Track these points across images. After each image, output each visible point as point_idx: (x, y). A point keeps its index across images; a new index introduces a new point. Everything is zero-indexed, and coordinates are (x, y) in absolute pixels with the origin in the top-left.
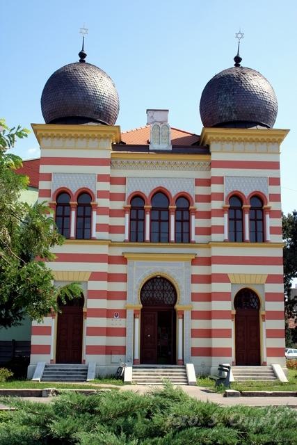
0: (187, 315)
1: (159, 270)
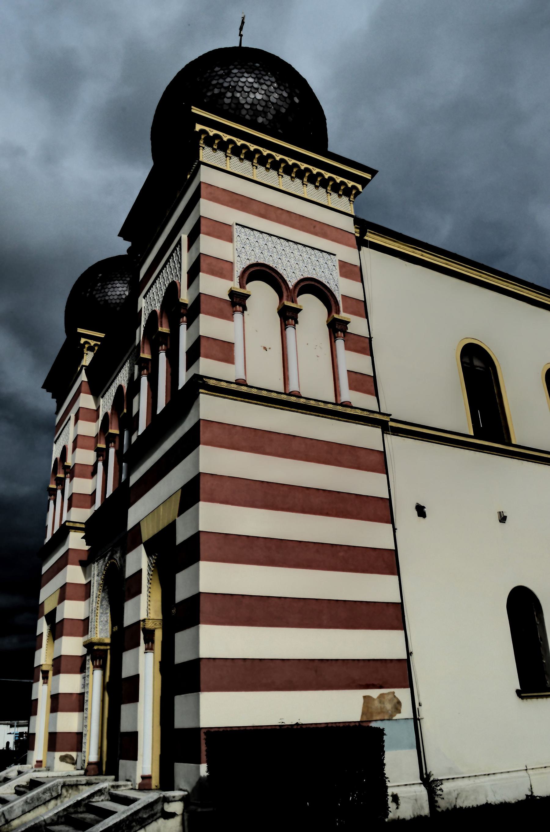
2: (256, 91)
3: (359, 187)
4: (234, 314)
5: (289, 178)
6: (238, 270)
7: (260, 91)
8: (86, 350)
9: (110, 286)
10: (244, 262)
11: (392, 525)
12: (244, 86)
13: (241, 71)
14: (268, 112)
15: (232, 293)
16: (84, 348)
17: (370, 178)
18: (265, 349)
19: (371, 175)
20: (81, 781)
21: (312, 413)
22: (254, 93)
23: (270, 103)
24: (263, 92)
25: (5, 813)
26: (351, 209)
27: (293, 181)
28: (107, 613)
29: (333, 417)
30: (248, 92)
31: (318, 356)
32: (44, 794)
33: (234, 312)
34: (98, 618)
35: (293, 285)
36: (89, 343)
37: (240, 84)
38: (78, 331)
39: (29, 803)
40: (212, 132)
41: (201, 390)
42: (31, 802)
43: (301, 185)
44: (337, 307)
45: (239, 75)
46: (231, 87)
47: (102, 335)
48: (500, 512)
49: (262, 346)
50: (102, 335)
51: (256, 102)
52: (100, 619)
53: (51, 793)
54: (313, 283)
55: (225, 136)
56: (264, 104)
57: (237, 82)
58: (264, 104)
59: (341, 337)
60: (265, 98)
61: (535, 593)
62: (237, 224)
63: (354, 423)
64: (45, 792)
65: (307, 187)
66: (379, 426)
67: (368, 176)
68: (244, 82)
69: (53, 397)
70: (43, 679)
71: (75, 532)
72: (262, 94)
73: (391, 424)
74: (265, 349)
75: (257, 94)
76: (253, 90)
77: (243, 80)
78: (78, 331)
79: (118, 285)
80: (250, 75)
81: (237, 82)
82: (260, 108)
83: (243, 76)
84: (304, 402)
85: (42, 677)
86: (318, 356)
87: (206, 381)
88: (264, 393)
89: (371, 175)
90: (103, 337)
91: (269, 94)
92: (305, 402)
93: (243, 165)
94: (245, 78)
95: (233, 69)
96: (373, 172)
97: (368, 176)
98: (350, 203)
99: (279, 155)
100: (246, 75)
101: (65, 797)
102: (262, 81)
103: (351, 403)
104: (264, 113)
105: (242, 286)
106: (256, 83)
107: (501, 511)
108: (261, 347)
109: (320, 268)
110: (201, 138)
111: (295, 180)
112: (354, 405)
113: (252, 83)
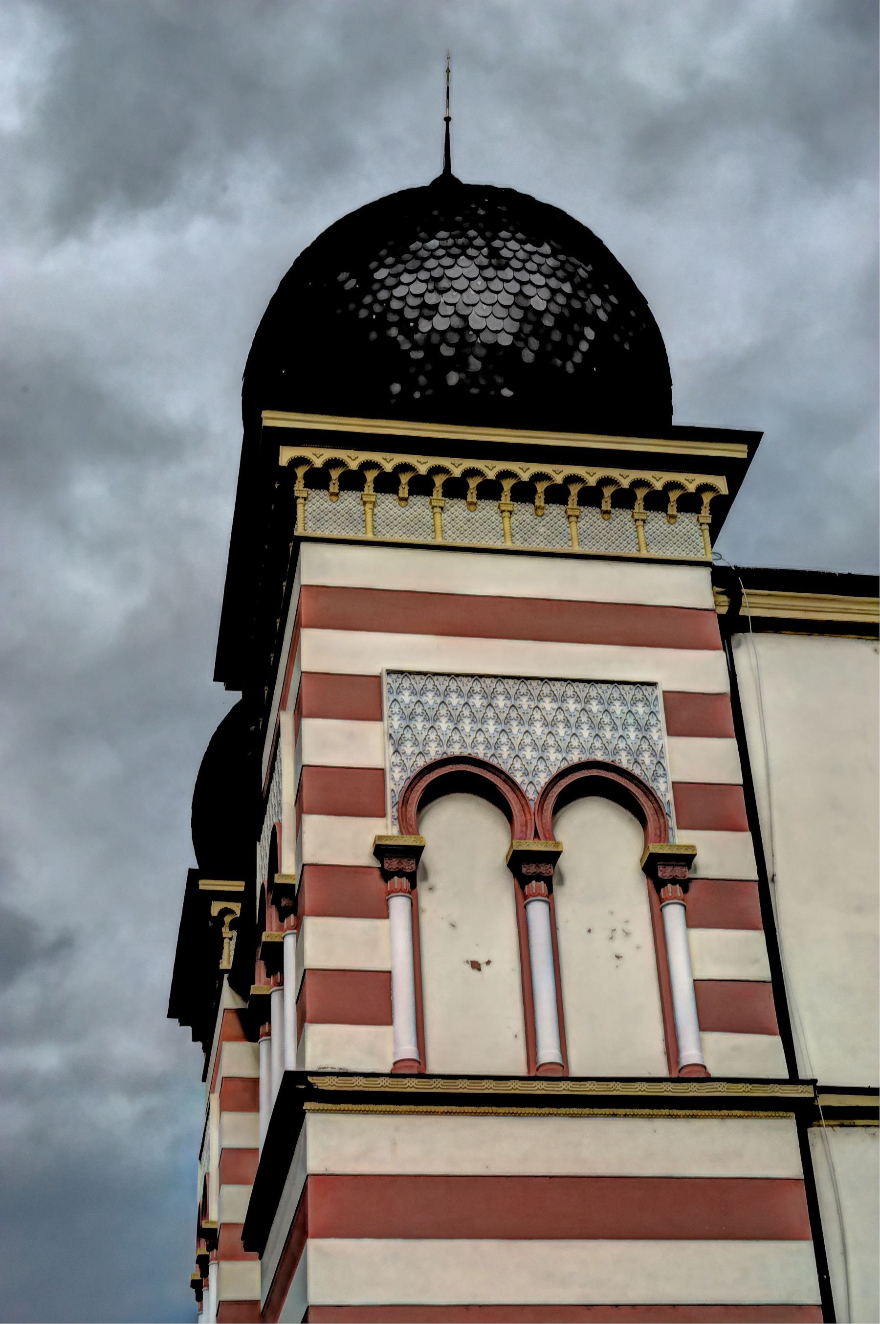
2: (432, 313)
3: (721, 483)
4: (389, 898)
5: (530, 510)
6: (396, 781)
7: (443, 309)
8: (228, 930)
10: (409, 764)
12: (404, 307)
13: (394, 270)
14: (469, 355)
15: (381, 851)
17: (744, 456)
18: (476, 966)
19: (746, 446)
21: (596, 1111)
22: (430, 318)
23: (471, 333)
24: (450, 310)
26: (705, 544)
27: (541, 516)
29: (655, 1112)
30: (415, 321)
31: (618, 957)
33: (389, 893)
35: (539, 792)
36: (231, 912)
37: (395, 305)
38: (201, 887)
40: (318, 456)
41: (307, 1106)
43: (564, 520)
44: (662, 821)
45: (391, 282)
46: (374, 317)
49: (467, 962)
51: (435, 338)
54: (594, 772)
55: (353, 458)
56: (454, 338)
57: (388, 301)
58: (454, 338)
59: (675, 898)
60: (457, 322)
62: (390, 672)
63: (715, 1117)
65: (579, 520)
66: (789, 1114)
67: (738, 451)
68: (403, 299)
69: (195, 1039)
72: (449, 316)
73: (824, 1101)
74: (476, 966)
75: (437, 319)
76: (426, 312)
77: (400, 292)
78: (201, 887)
80: (415, 275)
81: (388, 301)
82: (447, 351)
83: (400, 283)
84: (568, 1090)
86: (618, 957)
87: (315, 1083)
88: (460, 1085)
89: (746, 446)
91: (464, 311)
92: (570, 1089)
93: (408, 513)
94: (405, 286)
95: (377, 269)
96: (752, 439)
97: (738, 451)
98: (700, 529)
99: (494, 463)
100: (406, 278)
102: (444, 284)
103: (705, 1067)
104: (459, 362)
105: (407, 825)
106: (431, 292)
108: (467, 964)
109: (615, 728)
110: (295, 477)
111: (546, 512)
112: (714, 1072)
113: (422, 295)
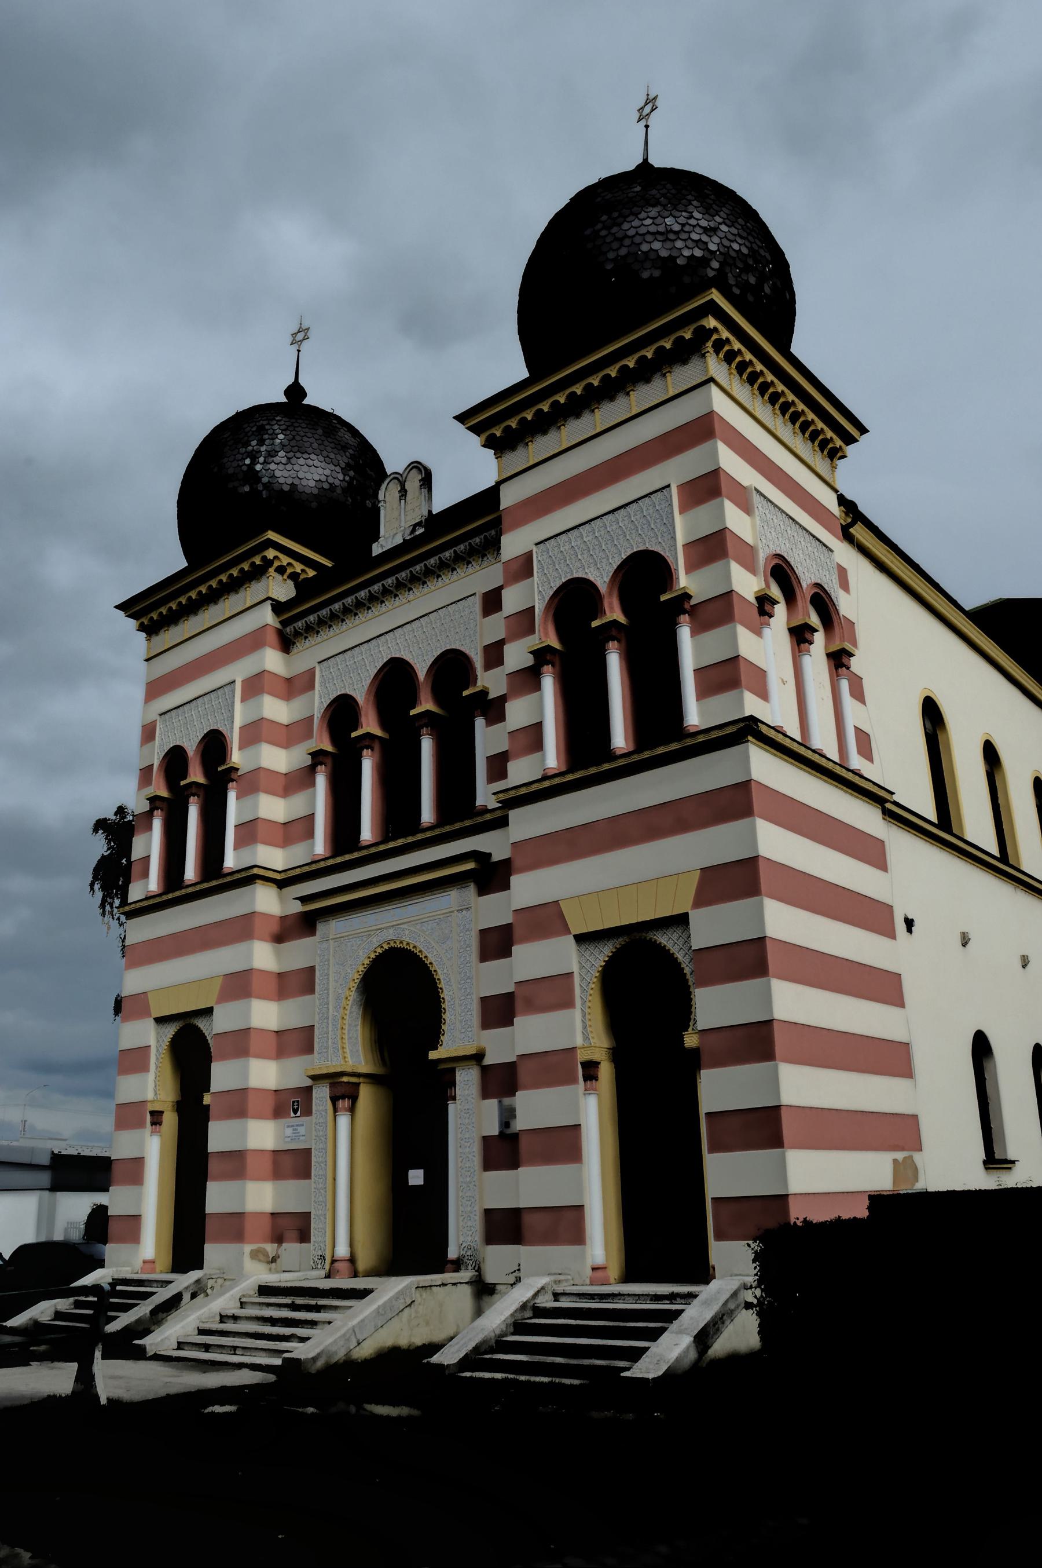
0: (467, 1080)
1: (390, 935)
9: (302, 461)
11: (632, 750)
16: (271, 567)
20: (435, 1281)
25: (356, 1329)
28: (356, 1026)
32: (397, 1300)
34: (346, 1032)
39: (382, 1315)
42: (383, 1313)
47: (328, 563)
48: (964, 933)
50: (328, 563)
52: (349, 1034)
53: (405, 1299)
61: (998, 744)
64: (398, 1298)
70: (585, 1080)
71: (263, 884)
79: (316, 463)
85: (583, 1075)
90: (330, 565)
101: (420, 1304)
107: (965, 930)
